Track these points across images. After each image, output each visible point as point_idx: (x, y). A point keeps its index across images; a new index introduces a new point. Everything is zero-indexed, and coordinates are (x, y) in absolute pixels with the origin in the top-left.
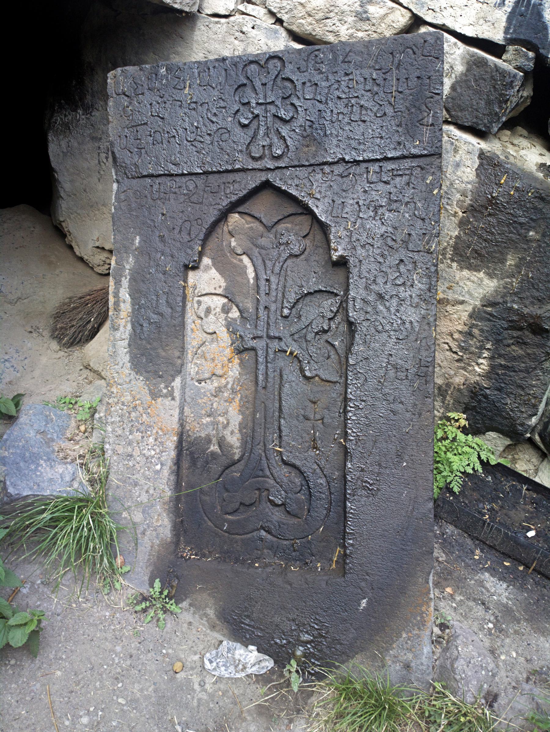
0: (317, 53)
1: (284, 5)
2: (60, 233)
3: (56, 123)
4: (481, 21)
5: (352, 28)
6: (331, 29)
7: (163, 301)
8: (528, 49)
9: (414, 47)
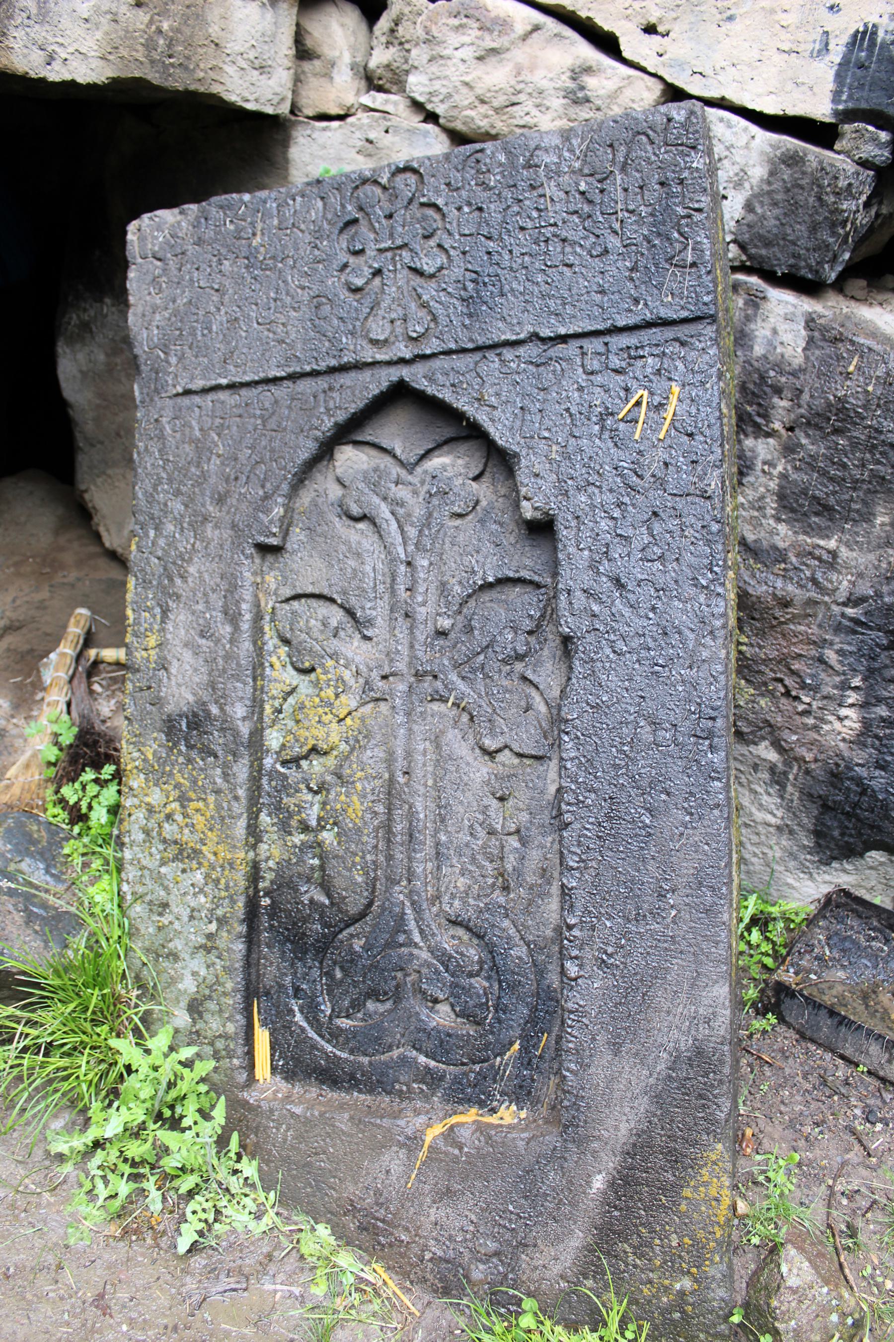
0: (479, 155)
1: (435, 88)
2: (82, 516)
3: (69, 323)
4: (790, 86)
5: (560, 118)
6: (522, 123)
8: (877, 127)
9: (650, 133)
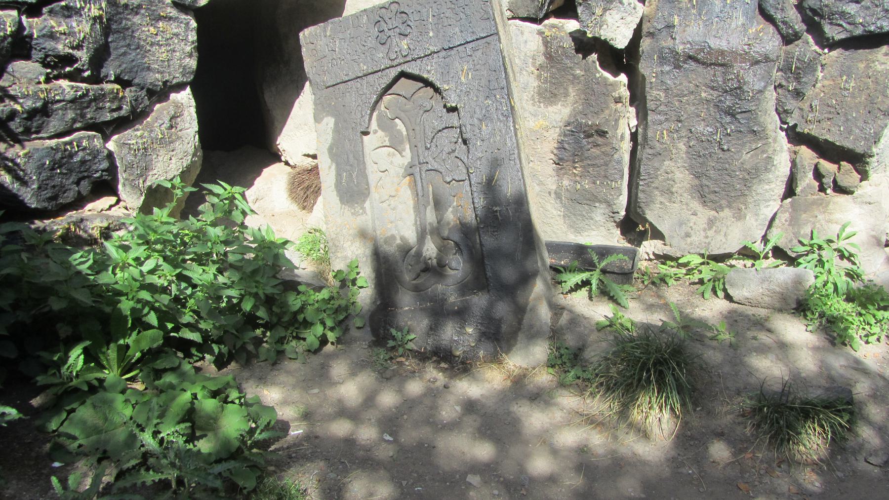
7: (351, 156)
